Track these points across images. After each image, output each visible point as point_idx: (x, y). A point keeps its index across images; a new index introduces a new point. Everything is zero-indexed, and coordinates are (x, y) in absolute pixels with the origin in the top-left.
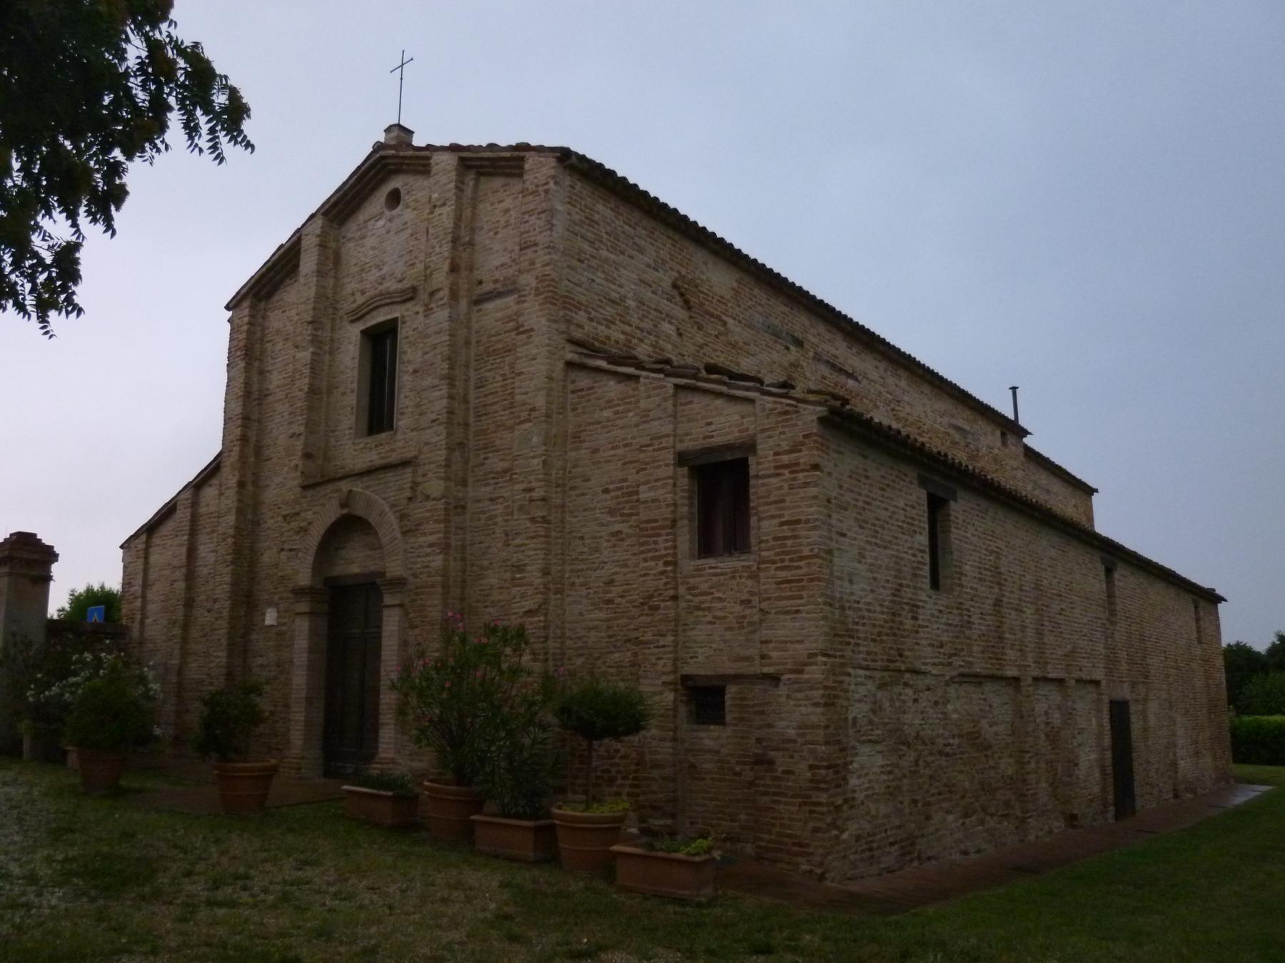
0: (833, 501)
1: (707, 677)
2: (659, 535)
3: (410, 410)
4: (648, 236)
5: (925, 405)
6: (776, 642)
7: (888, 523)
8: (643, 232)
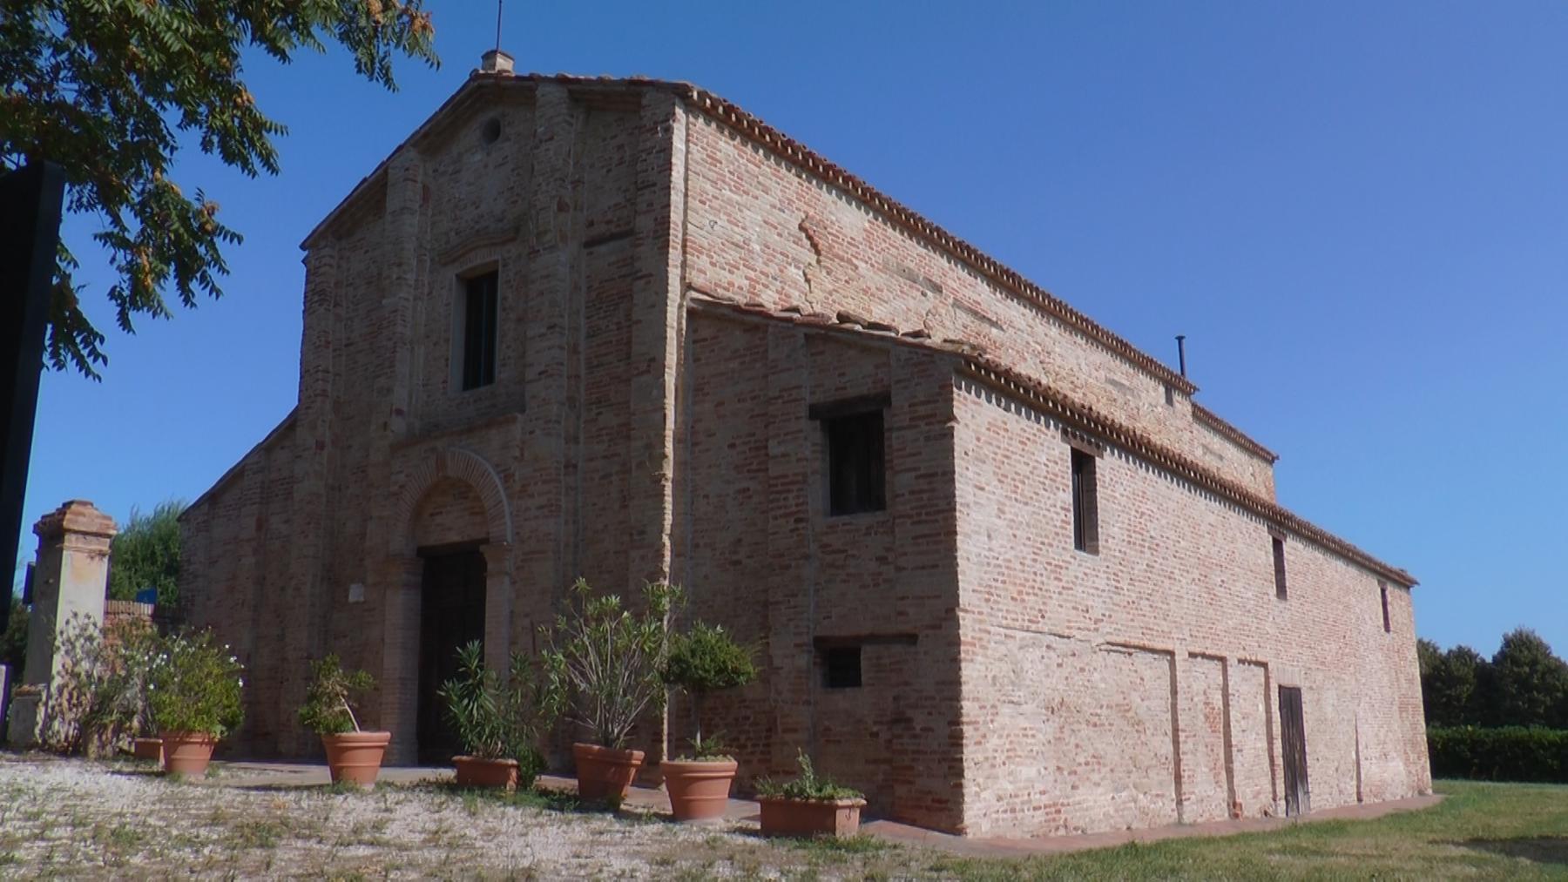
0: (970, 453)
2: (789, 491)
4: (774, 175)
5: (1078, 358)
8: (768, 170)
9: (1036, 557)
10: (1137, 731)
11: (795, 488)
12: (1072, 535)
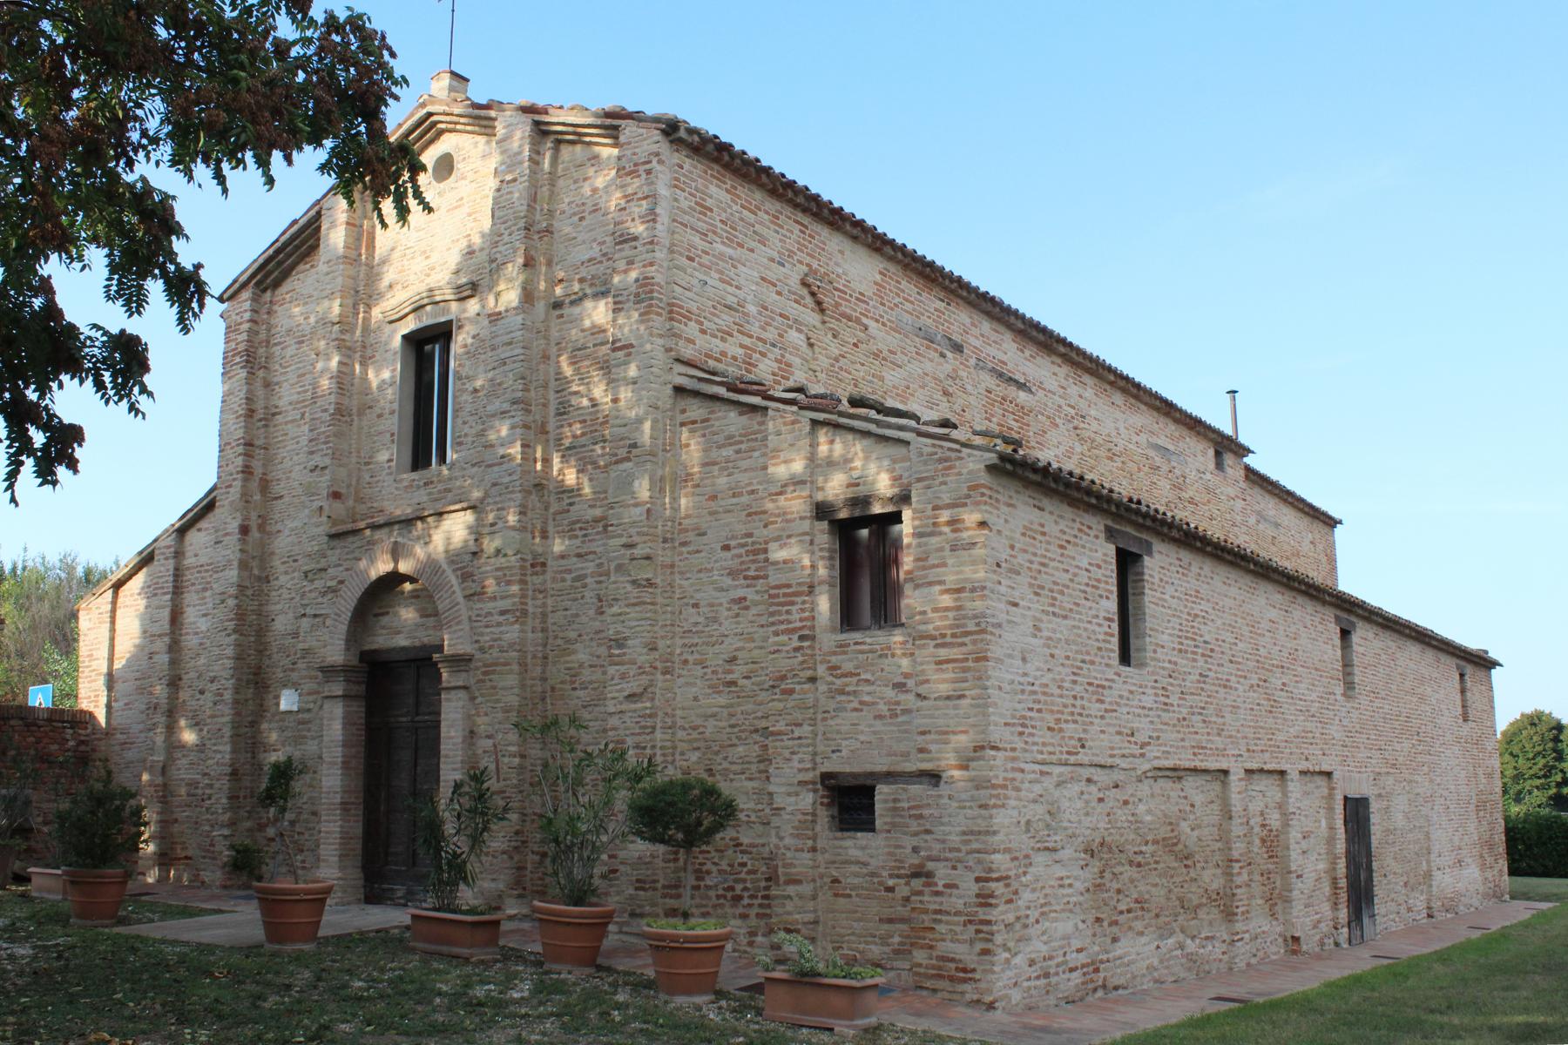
0: (1003, 565)
1: (853, 775)
2: (792, 603)
3: (470, 439)
4: (772, 222)
6: (936, 732)
7: (1068, 587)
8: (766, 217)
9: (1075, 678)
10: (1186, 866)
11: (799, 599)
12: (1116, 648)
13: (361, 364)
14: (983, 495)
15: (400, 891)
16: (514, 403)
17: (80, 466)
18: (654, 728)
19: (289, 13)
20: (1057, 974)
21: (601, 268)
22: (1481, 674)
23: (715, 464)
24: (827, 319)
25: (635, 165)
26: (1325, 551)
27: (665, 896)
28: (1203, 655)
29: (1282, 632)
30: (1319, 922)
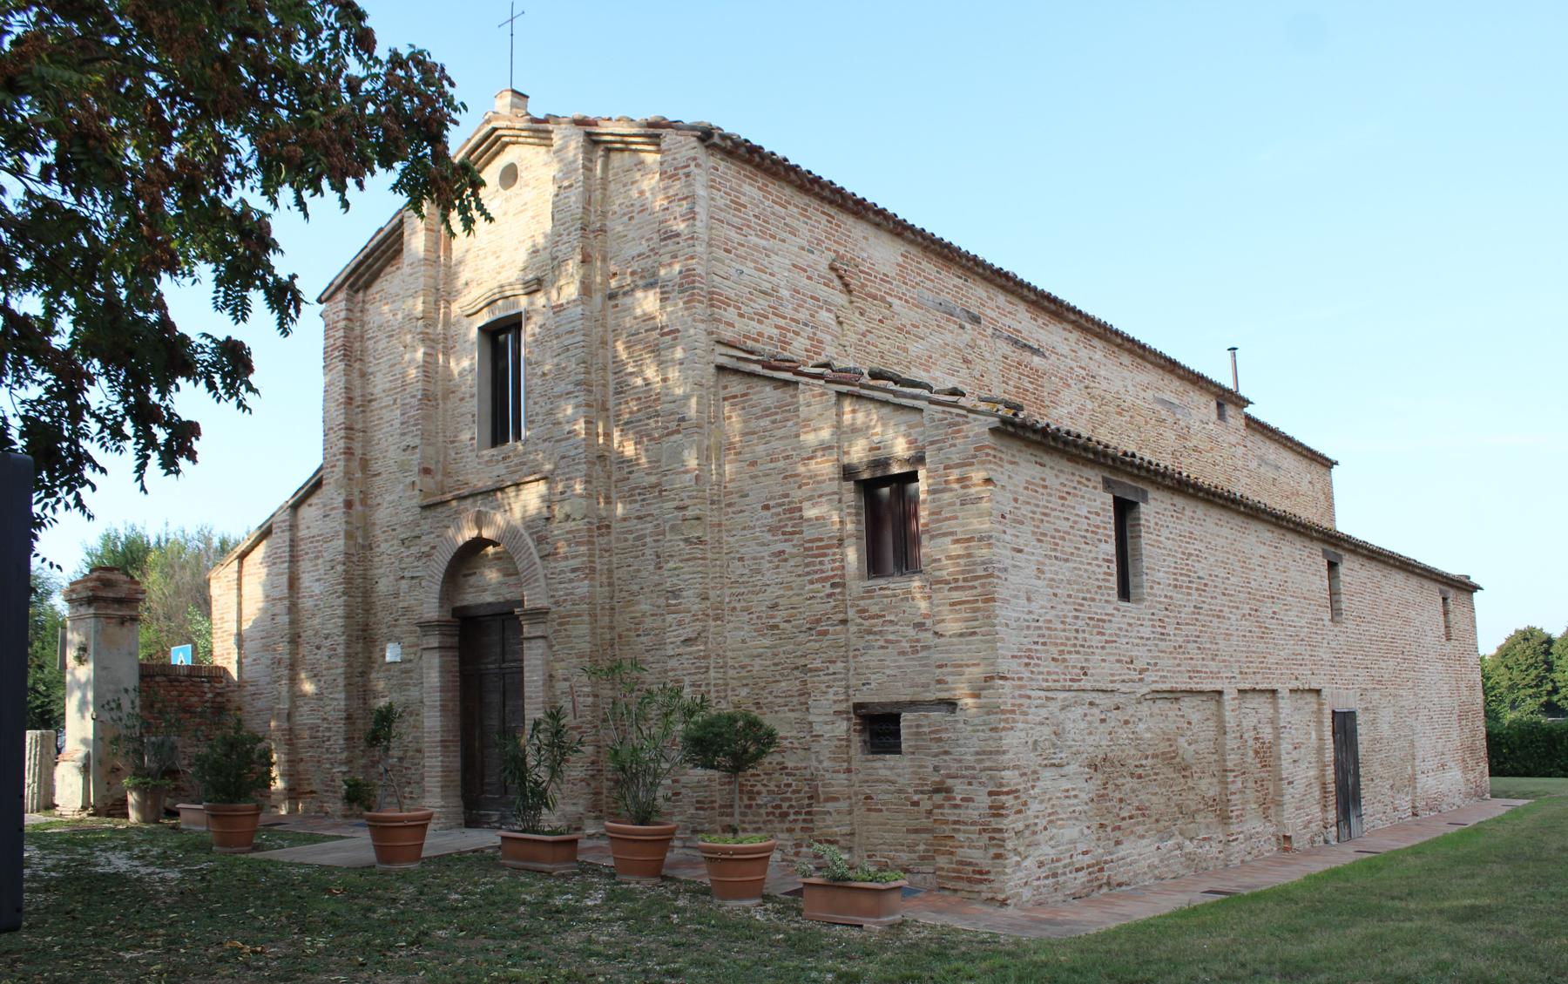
0: (1008, 516)
1: (880, 704)
2: (825, 555)
3: (540, 417)
4: (801, 214)
5: (1124, 379)
8: (795, 210)
11: (830, 551)
12: (1115, 586)
13: (444, 354)
14: (987, 455)
15: (495, 817)
16: (577, 385)
17: (198, 457)
18: (708, 668)
19: (356, 54)
20: (1064, 874)
21: (650, 262)
22: (1463, 597)
23: (754, 433)
24: (854, 299)
25: (676, 169)
26: (1323, 490)
27: (721, 814)
28: (1197, 589)
29: (1271, 566)
30: (1310, 822)
